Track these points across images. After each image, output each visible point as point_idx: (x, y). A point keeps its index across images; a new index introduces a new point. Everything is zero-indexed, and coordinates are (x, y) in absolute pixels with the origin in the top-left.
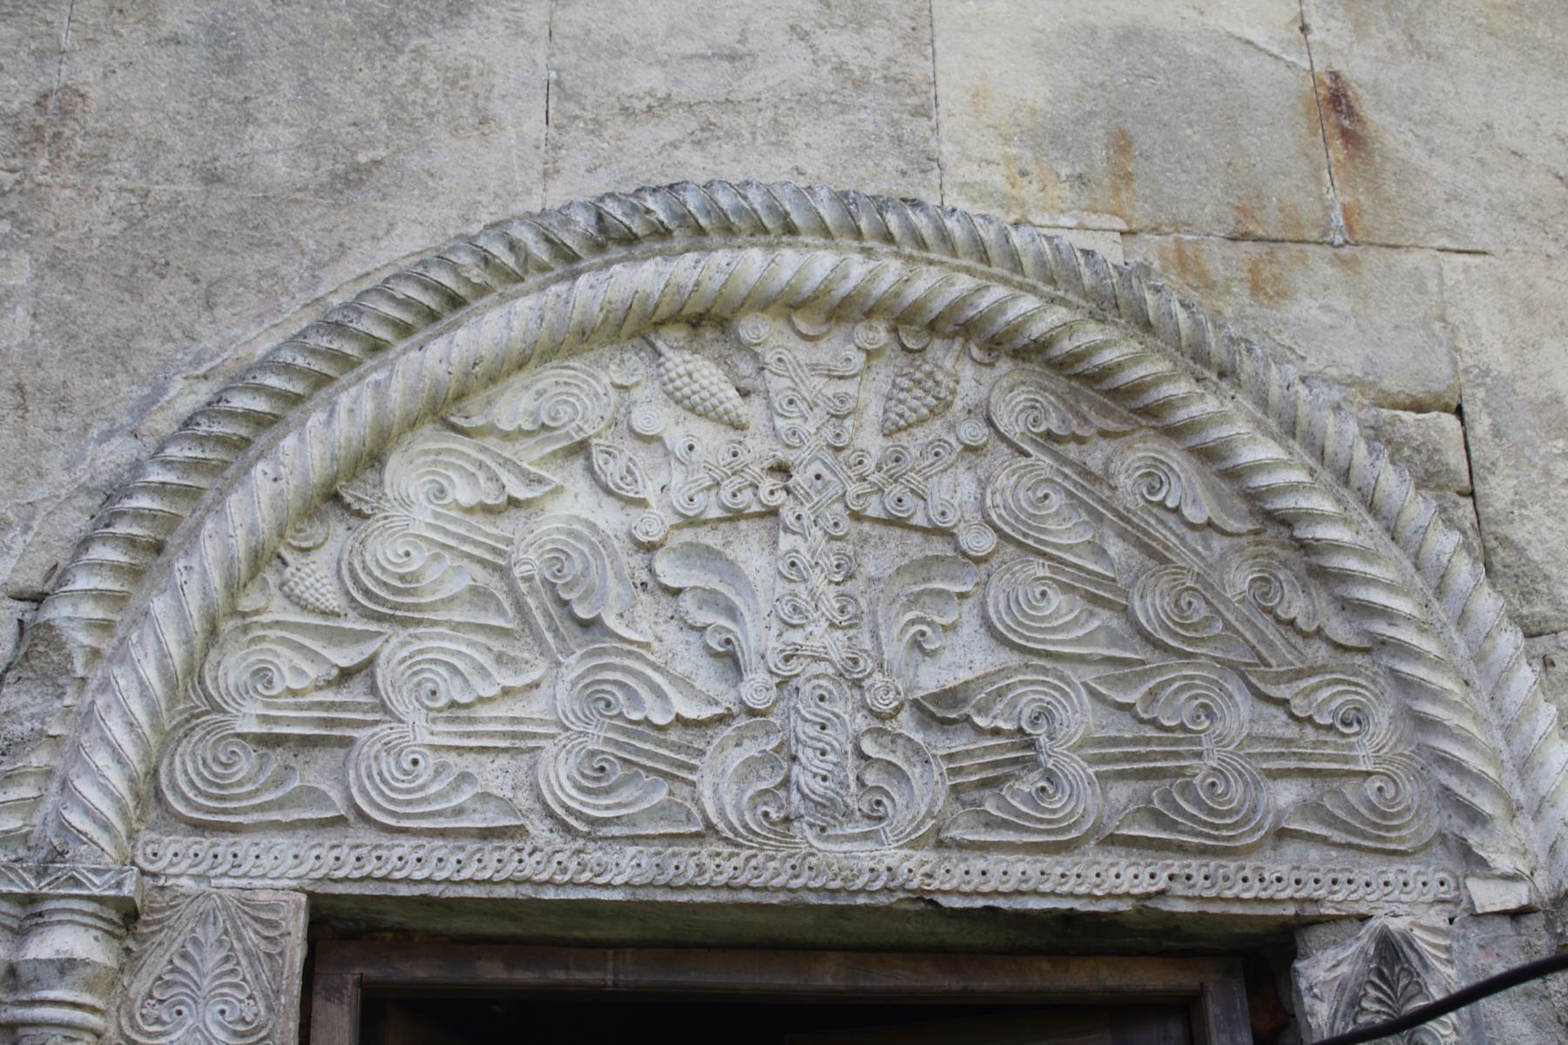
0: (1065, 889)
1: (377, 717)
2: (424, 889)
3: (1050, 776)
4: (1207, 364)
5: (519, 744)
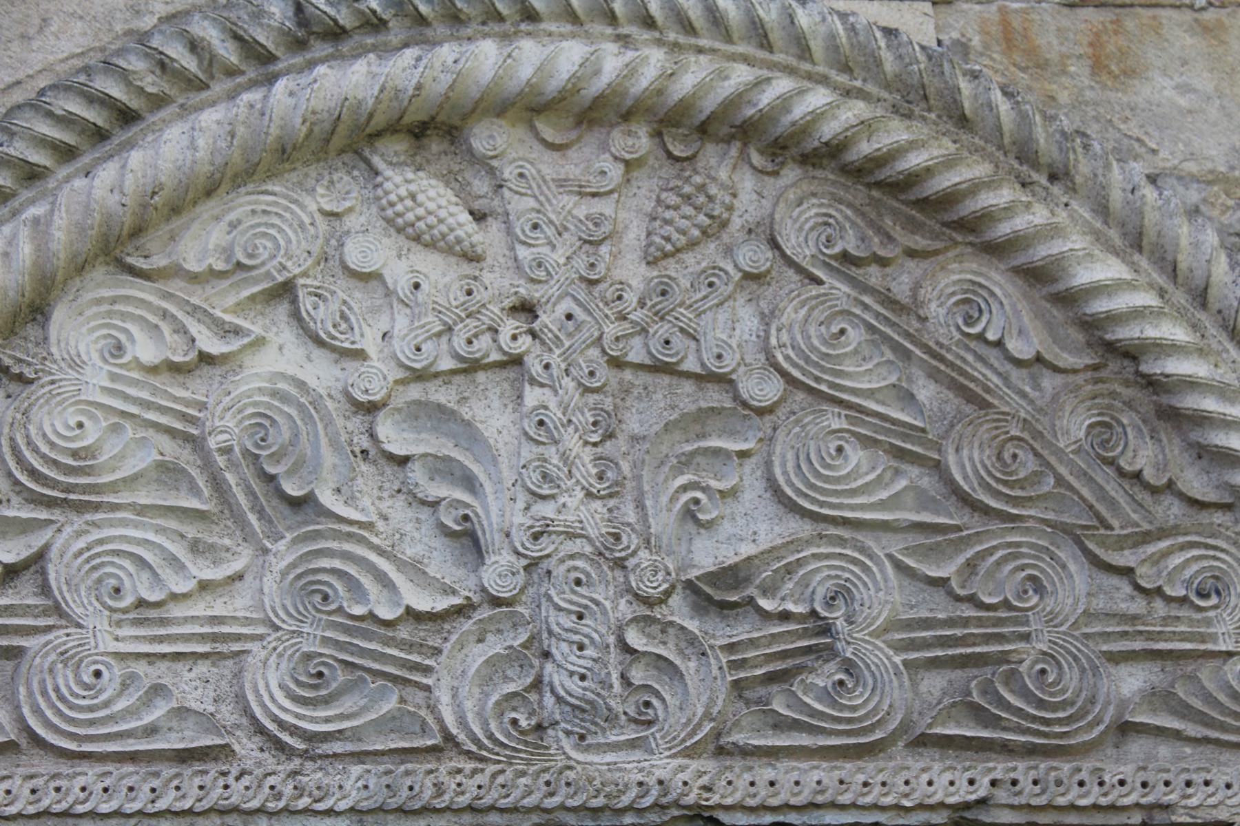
0: (868, 800)
1: (50, 622)
3: (849, 667)
4: (1036, 165)
5: (222, 648)
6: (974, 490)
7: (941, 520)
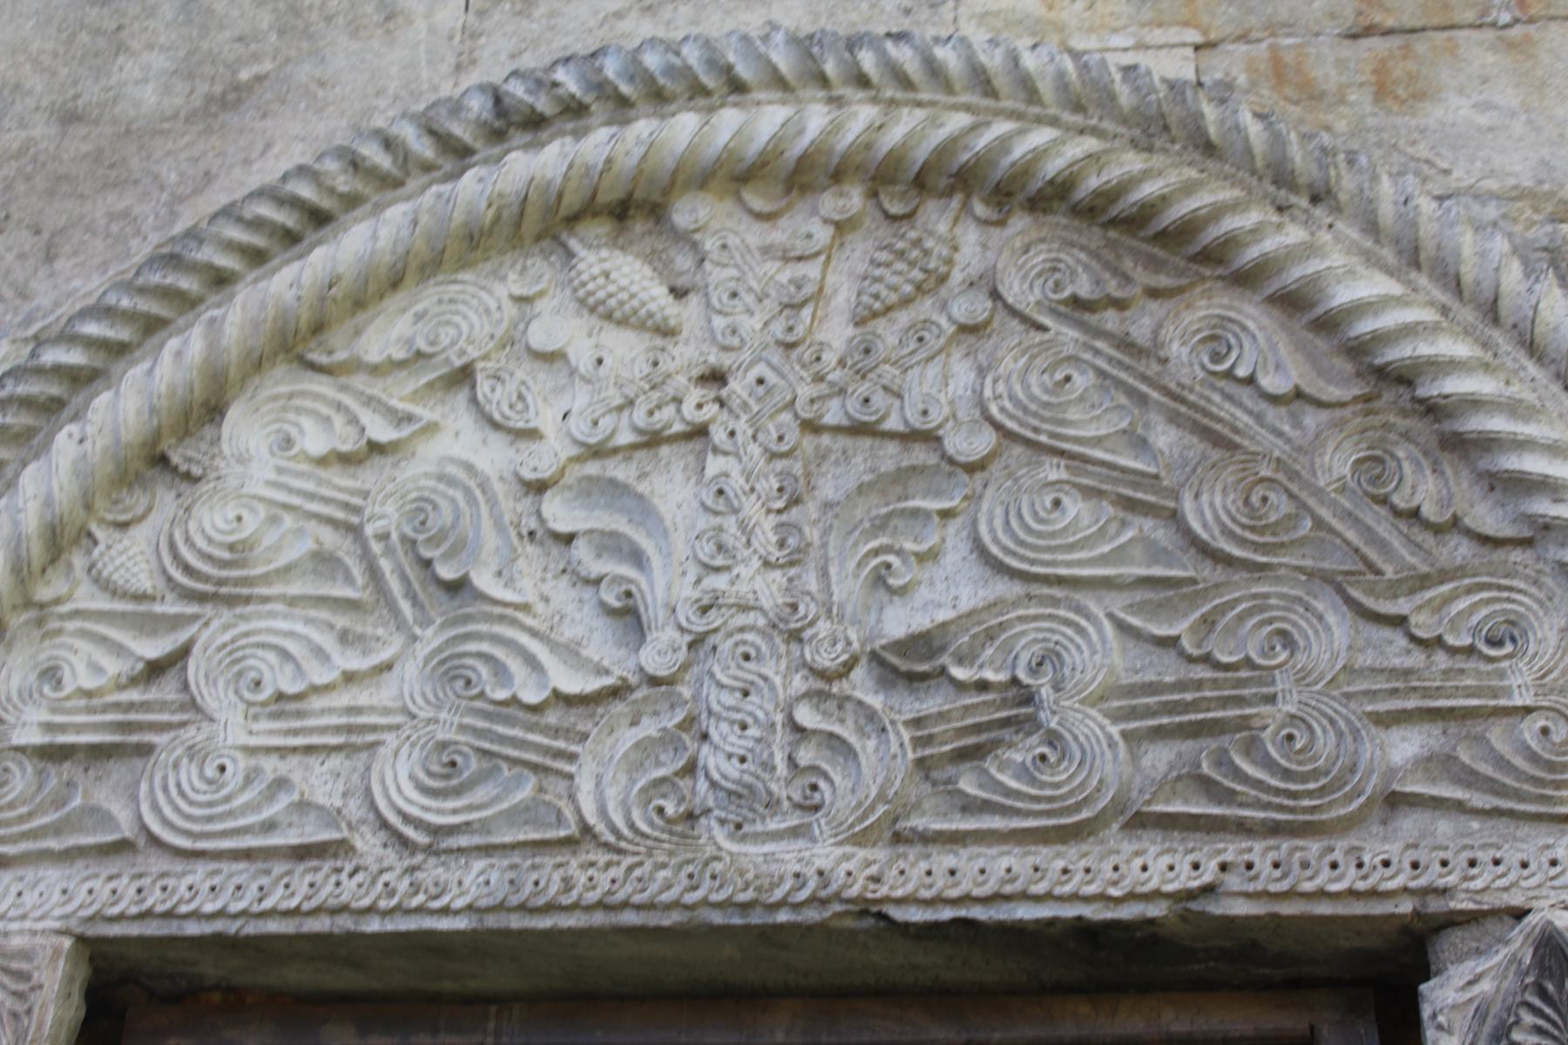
0: (1067, 889)
1: (185, 717)
2: (218, 926)
3: (1053, 739)
4: (1293, 187)
5: (356, 739)
6: (1214, 538)
7: (1175, 573)
